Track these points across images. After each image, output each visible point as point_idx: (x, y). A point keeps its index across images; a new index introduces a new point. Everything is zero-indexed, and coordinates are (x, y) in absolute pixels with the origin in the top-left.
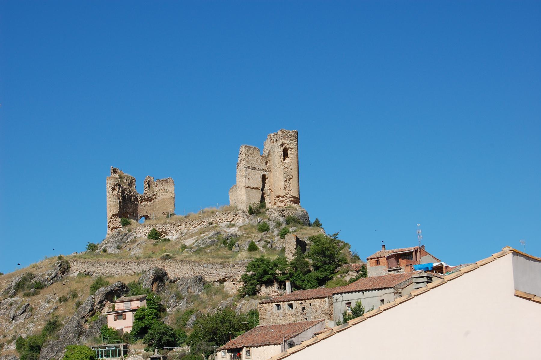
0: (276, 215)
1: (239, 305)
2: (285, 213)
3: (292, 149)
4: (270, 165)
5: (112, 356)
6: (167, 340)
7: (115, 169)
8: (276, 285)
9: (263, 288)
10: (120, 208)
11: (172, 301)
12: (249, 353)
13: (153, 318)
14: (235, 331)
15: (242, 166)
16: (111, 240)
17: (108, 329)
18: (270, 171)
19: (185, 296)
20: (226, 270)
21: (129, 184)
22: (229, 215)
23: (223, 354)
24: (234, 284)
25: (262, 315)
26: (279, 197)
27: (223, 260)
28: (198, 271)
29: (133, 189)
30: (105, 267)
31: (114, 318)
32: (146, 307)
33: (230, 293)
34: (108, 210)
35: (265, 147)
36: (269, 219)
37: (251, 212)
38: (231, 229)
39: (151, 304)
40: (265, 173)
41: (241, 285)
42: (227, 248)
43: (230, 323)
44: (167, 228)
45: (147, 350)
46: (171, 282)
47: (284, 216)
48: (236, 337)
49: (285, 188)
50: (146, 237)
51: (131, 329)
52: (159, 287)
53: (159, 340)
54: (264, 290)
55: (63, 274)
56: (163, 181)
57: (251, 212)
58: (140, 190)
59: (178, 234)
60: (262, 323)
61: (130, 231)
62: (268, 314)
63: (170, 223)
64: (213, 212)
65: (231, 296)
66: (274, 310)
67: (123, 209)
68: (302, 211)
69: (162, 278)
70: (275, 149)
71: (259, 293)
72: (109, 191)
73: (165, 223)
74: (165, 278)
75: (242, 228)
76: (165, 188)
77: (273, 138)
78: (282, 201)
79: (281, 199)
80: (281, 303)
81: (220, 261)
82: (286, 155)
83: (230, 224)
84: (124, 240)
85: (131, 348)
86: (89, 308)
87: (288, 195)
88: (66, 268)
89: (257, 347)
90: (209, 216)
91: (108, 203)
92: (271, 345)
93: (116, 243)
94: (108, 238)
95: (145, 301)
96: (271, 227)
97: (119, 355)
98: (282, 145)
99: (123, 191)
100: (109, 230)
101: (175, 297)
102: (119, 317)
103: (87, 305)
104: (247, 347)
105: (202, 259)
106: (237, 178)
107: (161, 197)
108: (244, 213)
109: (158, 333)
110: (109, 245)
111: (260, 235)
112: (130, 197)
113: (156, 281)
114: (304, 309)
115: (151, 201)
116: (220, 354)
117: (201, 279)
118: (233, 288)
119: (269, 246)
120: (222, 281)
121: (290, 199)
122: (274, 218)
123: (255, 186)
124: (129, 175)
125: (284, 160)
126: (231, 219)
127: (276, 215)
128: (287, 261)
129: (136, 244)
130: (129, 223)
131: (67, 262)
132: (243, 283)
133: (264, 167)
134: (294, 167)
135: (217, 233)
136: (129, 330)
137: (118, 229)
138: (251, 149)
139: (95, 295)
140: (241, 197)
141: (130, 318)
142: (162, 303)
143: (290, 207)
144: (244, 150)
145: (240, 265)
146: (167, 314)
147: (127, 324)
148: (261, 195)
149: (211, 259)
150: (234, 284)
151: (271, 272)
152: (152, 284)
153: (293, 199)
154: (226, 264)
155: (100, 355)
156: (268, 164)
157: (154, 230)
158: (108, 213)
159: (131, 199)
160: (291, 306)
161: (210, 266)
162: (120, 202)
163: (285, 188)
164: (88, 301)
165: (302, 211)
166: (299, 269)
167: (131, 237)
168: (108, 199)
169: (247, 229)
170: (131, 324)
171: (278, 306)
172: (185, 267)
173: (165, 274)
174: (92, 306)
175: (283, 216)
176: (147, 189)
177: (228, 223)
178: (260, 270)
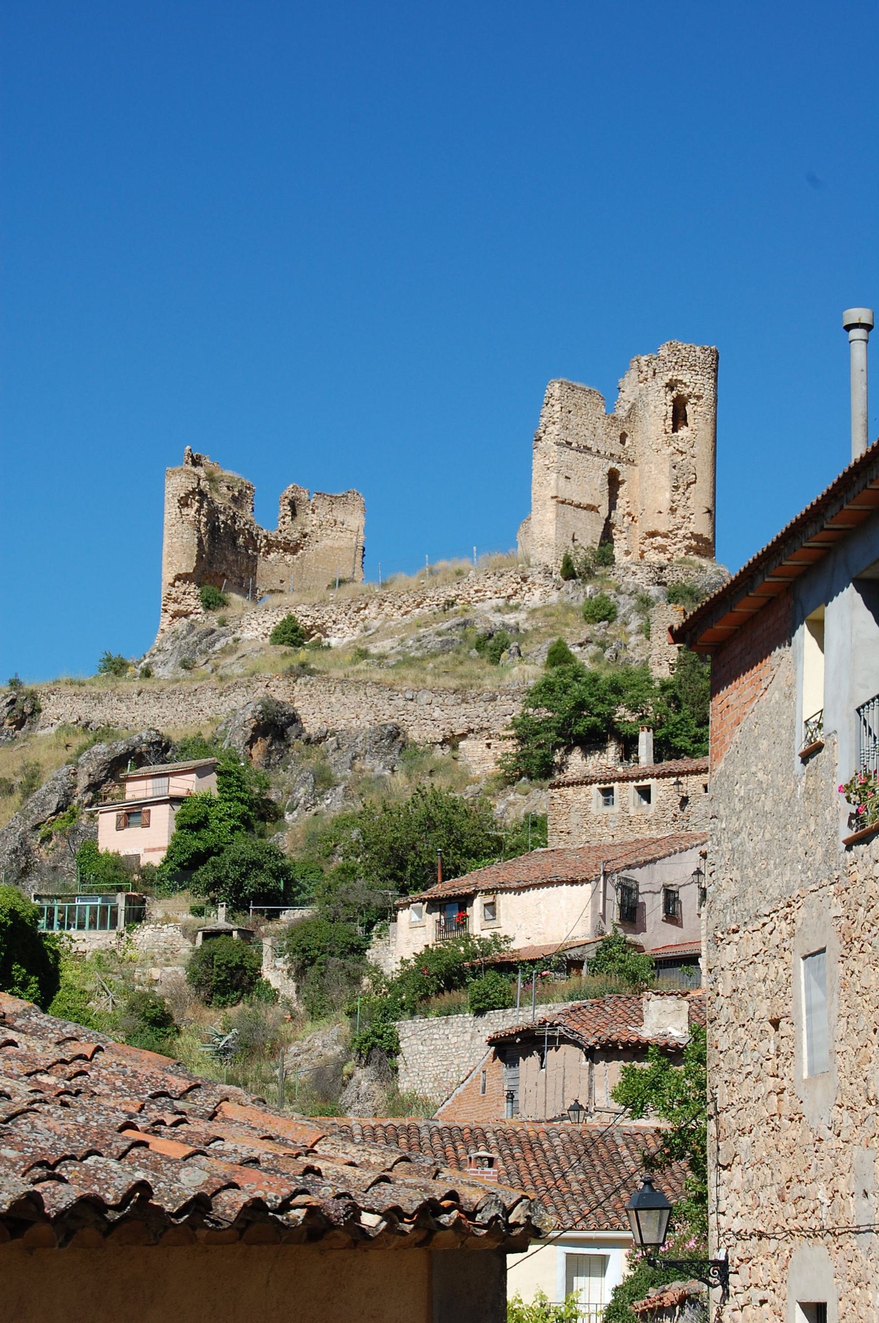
0: (641, 579)
1: (500, 806)
2: (668, 576)
3: (699, 398)
4: (632, 445)
5: (93, 925)
6: (264, 885)
7: (199, 457)
8: (612, 749)
9: (576, 758)
10: (199, 558)
11: (302, 790)
12: (494, 913)
13: (234, 829)
14: (463, 855)
15: (548, 442)
16: (168, 646)
17: (99, 856)
18: (631, 462)
19: (344, 778)
20: (470, 709)
21: (234, 499)
22: (504, 580)
23: (415, 917)
24: (489, 745)
25: (557, 824)
26: (653, 534)
27: (464, 682)
28: (389, 713)
29: (247, 514)
30: (132, 706)
31: (118, 823)
32: (216, 795)
33: (477, 771)
34: (165, 560)
35: (622, 395)
36: (617, 589)
37: (569, 573)
38: (507, 616)
39: (230, 786)
40: (618, 467)
41: (510, 747)
42: (485, 660)
43: (450, 832)
44: (325, 615)
45: (199, 912)
46: (308, 741)
47: (665, 584)
48: (464, 873)
49: (673, 510)
50: (267, 640)
51: (163, 854)
52: (270, 752)
53: (238, 887)
54: (577, 763)
55: (19, 727)
56: (333, 500)
57: (569, 573)
58: (266, 519)
59: (357, 632)
60: (554, 842)
61: (223, 623)
62: (575, 819)
63: (338, 604)
64: (459, 573)
65: (476, 781)
66: (592, 807)
67: (210, 563)
68: (718, 573)
69: (283, 731)
70: (650, 398)
71: (561, 771)
72: (171, 509)
73: (324, 602)
74: (292, 730)
75: (538, 614)
76: (339, 520)
77: (645, 368)
78: (662, 549)
79: (659, 540)
80: (616, 785)
81: (453, 683)
82: (679, 418)
83: (507, 605)
84: (202, 646)
85: (156, 909)
86: (55, 800)
87: (681, 532)
88: (28, 710)
89: (519, 890)
90: (446, 582)
91: (166, 541)
92: (560, 883)
93: (181, 653)
94: (162, 641)
95: (214, 777)
96: (621, 611)
97: (114, 925)
98: (671, 386)
99: (213, 513)
100: (165, 619)
101: (311, 780)
102: (132, 819)
103: (51, 791)
104: (487, 892)
105: (404, 678)
106: (534, 475)
107: (326, 542)
108: (548, 573)
109: (234, 862)
110: (160, 658)
111: (587, 630)
112: (233, 535)
113: (264, 736)
114: (685, 801)
115: (294, 551)
116: (404, 916)
117: (395, 734)
118: (482, 758)
119: (607, 654)
120: (452, 741)
121: (687, 542)
122: (631, 588)
123: (585, 501)
124: (237, 476)
125: (675, 430)
126: (510, 592)
127: (641, 579)
128: (651, 682)
129: (235, 656)
130: (224, 603)
131: (33, 696)
132: (516, 741)
133: (617, 449)
134: (703, 450)
135: (465, 624)
136: (156, 859)
137: (192, 617)
138: (579, 394)
139: (77, 765)
140: (546, 534)
141: (163, 819)
142: (273, 797)
143: (682, 561)
144: (557, 394)
145: (513, 696)
146: (283, 828)
147: (149, 842)
148: (601, 529)
149: (429, 679)
150: (489, 745)
151: (600, 709)
152: (251, 743)
153: (694, 543)
154: (473, 692)
155: (56, 923)
156: (628, 443)
157: (291, 618)
158: (165, 570)
159: (235, 539)
160: (645, 793)
161: (425, 697)
162: (200, 541)
163: (673, 510)
164: (56, 779)
165: (718, 573)
166: (685, 706)
167: (223, 641)
168: (166, 532)
169: (552, 615)
170: (164, 841)
171: (607, 793)
172: (353, 698)
173: (294, 719)
174: (68, 797)
175: (659, 584)
176: (288, 519)
177: (501, 602)
178: (568, 703)
